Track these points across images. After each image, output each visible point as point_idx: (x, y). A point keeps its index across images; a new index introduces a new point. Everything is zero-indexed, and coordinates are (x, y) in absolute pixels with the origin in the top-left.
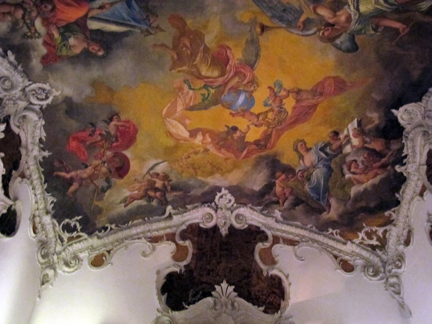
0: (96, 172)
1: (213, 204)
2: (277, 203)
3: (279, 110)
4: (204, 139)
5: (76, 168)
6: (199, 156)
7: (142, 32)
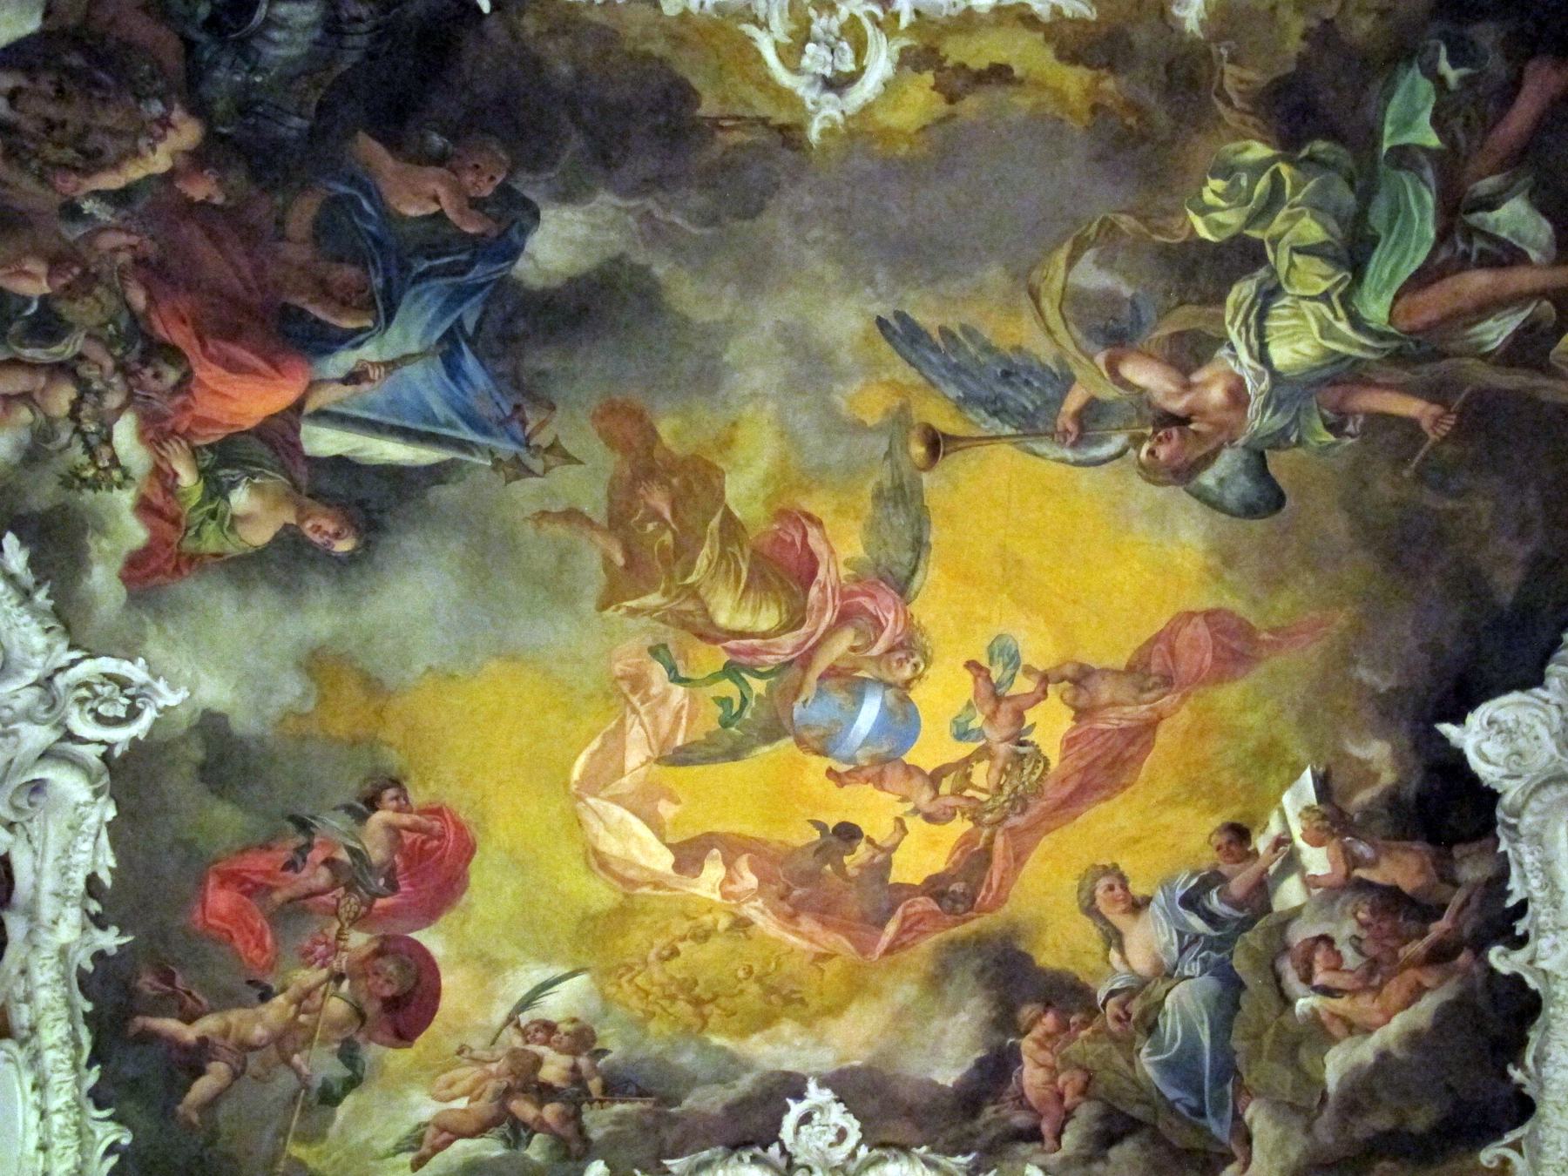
0: (302, 1018)
1: (774, 1150)
2: (1032, 1135)
3: (1016, 754)
4: (729, 879)
5: (226, 1000)
6: (716, 946)
7: (497, 464)
